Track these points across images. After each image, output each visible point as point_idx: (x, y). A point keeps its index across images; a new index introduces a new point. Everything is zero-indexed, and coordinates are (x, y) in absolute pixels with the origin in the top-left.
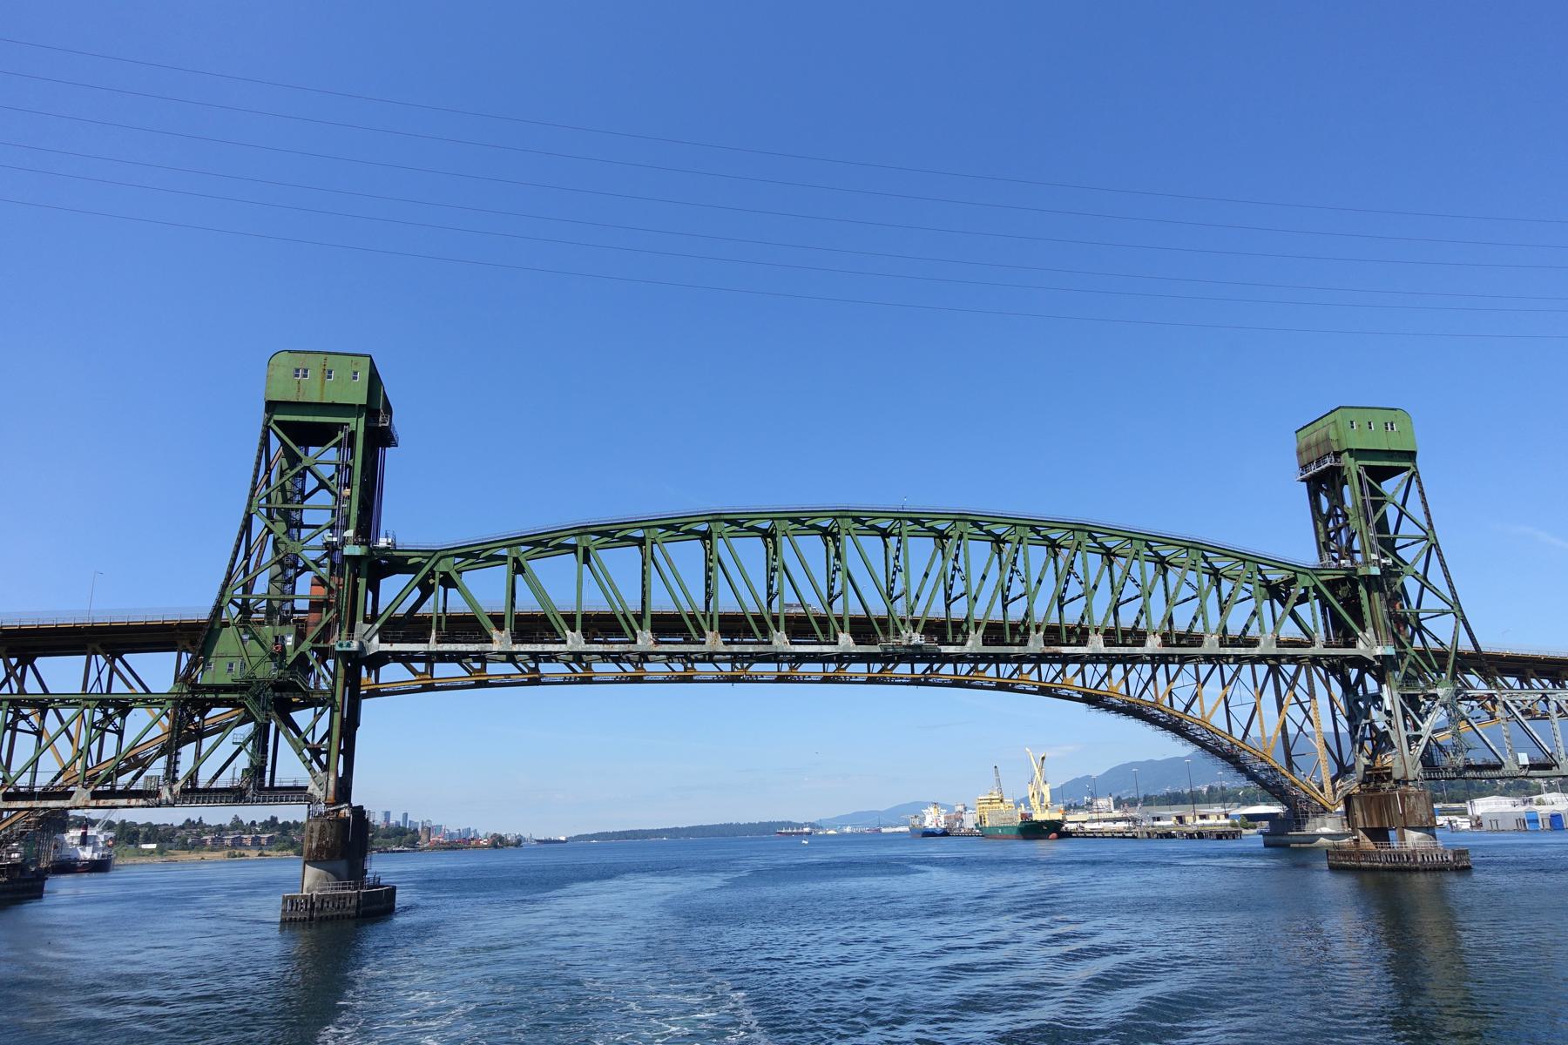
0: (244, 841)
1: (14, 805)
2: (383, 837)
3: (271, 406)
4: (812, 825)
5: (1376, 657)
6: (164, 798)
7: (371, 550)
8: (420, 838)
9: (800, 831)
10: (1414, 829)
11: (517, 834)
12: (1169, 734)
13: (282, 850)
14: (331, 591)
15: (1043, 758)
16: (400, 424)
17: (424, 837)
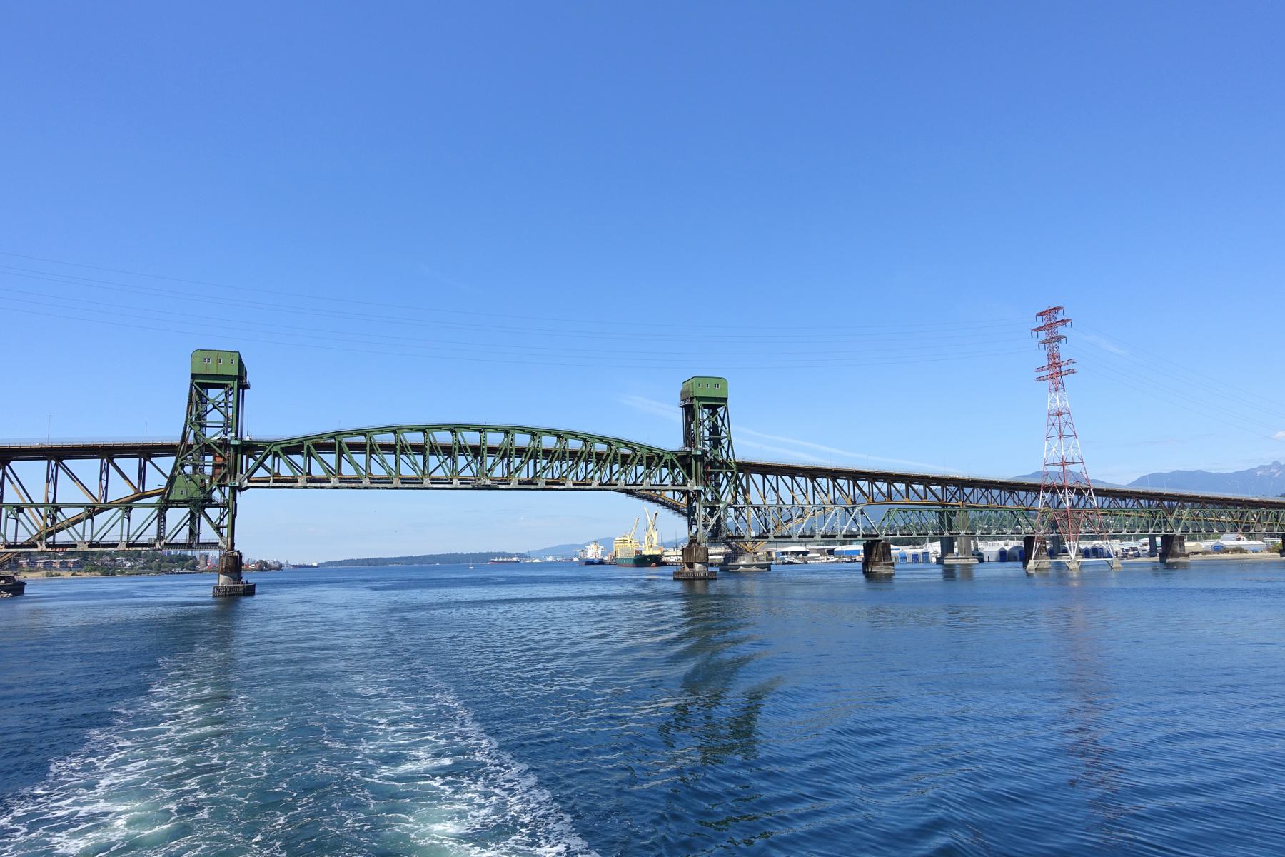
0: (54, 565)
1: (93, 549)
2: (168, 562)
3: (194, 376)
4: (520, 555)
5: (695, 491)
6: (157, 547)
7: (242, 442)
8: (198, 563)
9: (510, 560)
10: (699, 563)
11: (275, 560)
12: (671, 511)
13: (90, 571)
14: (225, 460)
15: (656, 514)
16: (250, 379)
17: (202, 562)
